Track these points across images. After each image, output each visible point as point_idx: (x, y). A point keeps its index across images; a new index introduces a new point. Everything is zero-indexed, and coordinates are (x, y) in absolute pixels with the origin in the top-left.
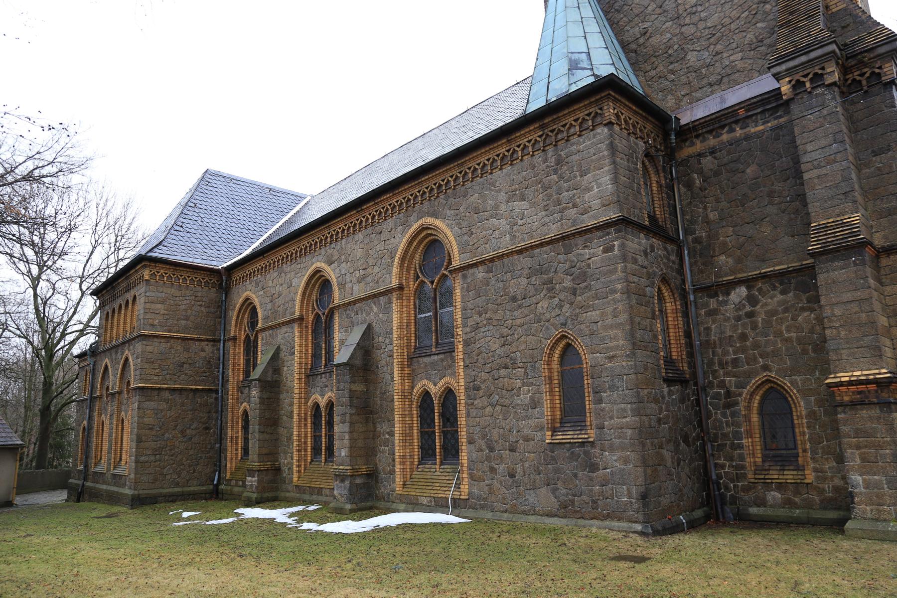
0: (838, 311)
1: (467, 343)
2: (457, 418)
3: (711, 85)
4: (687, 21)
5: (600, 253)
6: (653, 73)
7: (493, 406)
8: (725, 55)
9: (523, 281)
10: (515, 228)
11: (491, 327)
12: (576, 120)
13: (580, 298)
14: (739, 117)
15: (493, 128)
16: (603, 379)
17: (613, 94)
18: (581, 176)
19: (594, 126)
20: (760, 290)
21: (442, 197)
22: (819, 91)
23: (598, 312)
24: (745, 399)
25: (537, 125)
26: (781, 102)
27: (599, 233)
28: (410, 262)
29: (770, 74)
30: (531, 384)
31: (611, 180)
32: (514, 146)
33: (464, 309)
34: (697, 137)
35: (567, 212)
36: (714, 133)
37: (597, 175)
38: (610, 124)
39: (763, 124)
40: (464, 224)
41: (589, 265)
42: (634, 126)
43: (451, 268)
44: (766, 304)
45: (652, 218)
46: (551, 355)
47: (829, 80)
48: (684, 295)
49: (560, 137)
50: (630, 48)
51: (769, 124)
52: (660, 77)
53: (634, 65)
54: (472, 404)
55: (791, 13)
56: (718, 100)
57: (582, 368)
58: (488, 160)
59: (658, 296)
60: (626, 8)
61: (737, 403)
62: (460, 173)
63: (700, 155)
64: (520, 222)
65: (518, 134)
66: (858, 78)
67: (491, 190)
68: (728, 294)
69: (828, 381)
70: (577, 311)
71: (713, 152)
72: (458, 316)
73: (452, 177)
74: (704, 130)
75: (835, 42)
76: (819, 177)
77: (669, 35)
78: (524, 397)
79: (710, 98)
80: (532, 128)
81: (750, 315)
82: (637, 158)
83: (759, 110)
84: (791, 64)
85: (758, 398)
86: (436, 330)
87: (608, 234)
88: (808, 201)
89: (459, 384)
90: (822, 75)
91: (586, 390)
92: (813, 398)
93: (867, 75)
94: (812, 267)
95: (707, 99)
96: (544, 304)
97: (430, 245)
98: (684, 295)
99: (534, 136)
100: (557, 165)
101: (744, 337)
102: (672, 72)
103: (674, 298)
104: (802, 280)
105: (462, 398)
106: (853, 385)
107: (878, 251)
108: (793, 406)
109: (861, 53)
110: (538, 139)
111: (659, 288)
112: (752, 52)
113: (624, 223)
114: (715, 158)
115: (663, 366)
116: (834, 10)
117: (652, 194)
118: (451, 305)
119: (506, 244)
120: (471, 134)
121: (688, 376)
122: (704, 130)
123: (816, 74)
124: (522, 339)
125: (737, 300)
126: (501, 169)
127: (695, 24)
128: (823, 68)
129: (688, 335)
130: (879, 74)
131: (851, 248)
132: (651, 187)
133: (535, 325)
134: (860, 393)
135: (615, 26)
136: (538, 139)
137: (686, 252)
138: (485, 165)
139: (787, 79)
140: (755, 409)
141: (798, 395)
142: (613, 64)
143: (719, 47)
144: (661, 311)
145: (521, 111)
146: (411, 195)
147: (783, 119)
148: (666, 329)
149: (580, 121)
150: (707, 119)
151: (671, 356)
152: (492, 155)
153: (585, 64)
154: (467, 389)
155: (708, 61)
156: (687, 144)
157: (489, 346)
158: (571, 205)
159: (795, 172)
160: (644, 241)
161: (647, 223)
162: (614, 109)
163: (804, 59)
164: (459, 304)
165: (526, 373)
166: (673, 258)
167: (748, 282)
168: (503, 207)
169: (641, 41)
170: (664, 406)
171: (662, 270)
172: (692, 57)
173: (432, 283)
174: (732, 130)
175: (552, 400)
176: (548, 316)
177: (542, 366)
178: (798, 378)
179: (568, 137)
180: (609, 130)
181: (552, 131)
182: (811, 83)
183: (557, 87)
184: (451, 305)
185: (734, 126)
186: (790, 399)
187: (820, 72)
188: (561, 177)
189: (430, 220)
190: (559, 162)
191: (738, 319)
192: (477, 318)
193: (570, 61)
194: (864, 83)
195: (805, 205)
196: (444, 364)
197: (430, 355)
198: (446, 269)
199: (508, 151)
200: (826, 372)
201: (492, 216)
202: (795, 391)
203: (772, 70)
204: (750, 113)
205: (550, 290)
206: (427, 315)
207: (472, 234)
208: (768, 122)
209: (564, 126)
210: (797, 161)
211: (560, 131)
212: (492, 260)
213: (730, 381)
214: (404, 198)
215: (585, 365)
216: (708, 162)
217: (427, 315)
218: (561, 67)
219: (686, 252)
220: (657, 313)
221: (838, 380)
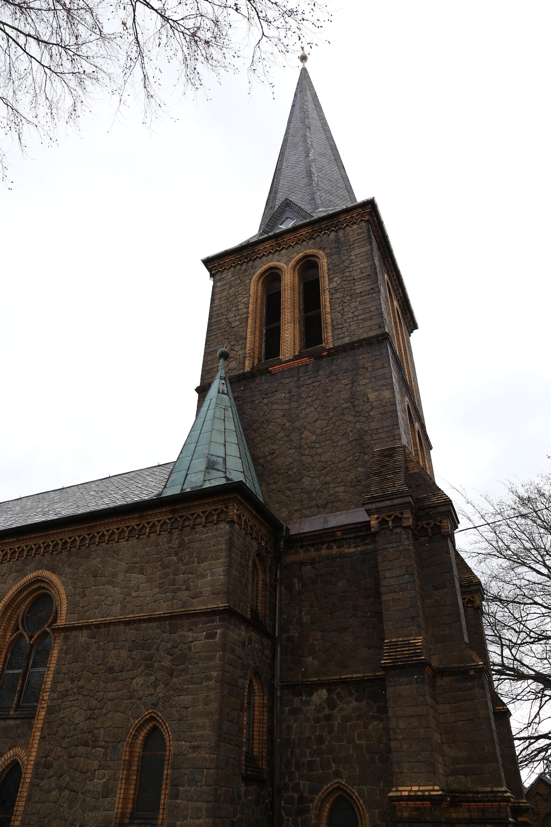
0: (402, 724)
1: (50, 711)
2: (15, 801)
3: (318, 507)
4: (307, 452)
5: (203, 638)
6: (274, 486)
7: (61, 789)
8: (332, 486)
9: (124, 653)
10: (128, 599)
11: (81, 697)
12: (204, 512)
13: (176, 680)
14: (336, 538)
15: (129, 500)
16: (184, 771)
17: (239, 497)
18: (199, 563)
19: (218, 521)
20: (338, 694)
21: (65, 553)
22: (398, 530)
23: (190, 697)
24: (317, 805)
25: (169, 509)
26: (370, 532)
27: (204, 619)
28: (14, 611)
29: (363, 509)
30: (108, 767)
31: (224, 571)
32: (144, 522)
33: (57, 672)
34: (302, 547)
35: (179, 593)
36: (315, 547)
37: (211, 570)
38: (232, 522)
39: (355, 547)
40: (80, 584)
41: (190, 649)
42: (251, 528)
43: (55, 626)
44: (342, 709)
45: (254, 612)
46: (135, 737)
47: (406, 523)
48: (272, 690)
49: (187, 523)
50: (258, 460)
51: (359, 549)
52: (279, 491)
53: (260, 476)
54: (38, 785)
55: (383, 467)
56: (322, 520)
57: (165, 755)
58: (118, 529)
59: (249, 688)
60: (261, 430)
61: (308, 811)
62: (88, 535)
63: (302, 563)
64: (134, 594)
65: (150, 513)
66: (425, 526)
67: (113, 557)
68: (311, 695)
69: (391, 794)
70: (171, 693)
71: (313, 562)
72: (49, 679)
73: (79, 536)
74: (308, 543)
75: (411, 496)
76: (393, 600)
77: (291, 460)
78: (98, 782)
79: (316, 517)
80: (164, 510)
81: (328, 718)
82: (249, 556)
83: (353, 535)
84: (380, 505)
85: (328, 806)
86: (21, 691)
87: (213, 621)
88: (384, 619)
89: (28, 757)
90: (401, 518)
91: (164, 782)
92: (377, 811)
93: (432, 525)
94: (382, 679)
95: (313, 518)
96: (140, 680)
97: (39, 599)
98: (272, 690)
99: (165, 518)
100: (179, 547)
101: (320, 740)
102: (289, 489)
103: (263, 692)
104: (373, 689)
105: (28, 777)
106: (411, 801)
107: (434, 672)
108: (359, 818)
109: (428, 508)
110: (167, 521)
111: (251, 681)
112: (352, 489)
113: (228, 614)
114: (314, 568)
115: (243, 763)
116: (412, 472)
117: (257, 590)
118: (45, 665)
119: (116, 613)
120: (106, 500)
121: (265, 775)
122: (308, 543)
123: (396, 517)
124: (109, 715)
125: (318, 702)
126: (127, 540)
127: (312, 456)
128: (402, 514)
129: (271, 731)
130: (439, 526)
131: (412, 667)
132: (257, 584)
133: (127, 701)
134: (417, 809)
135: (250, 441)
136: (167, 521)
137: (279, 649)
138: (113, 533)
139: (376, 516)
140: (325, 818)
141: (364, 806)
142: (243, 472)
143: (328, 478)
144: (249, 703)
145: (156, 492)
146: (35, 545)
147: (369, 547)
148: (251, 723)
149: (207, 513)
150: (312, 534)
151: (253, 751)
152: (122, 525)
153: (220, 467)
154: (37, 765)
155: (318, 487)
156: (293, 551)
157: (73, 717)
158: (184, 587)
159: (376, 593)
160: (243, 633)
161: (249, 616)
162: (238, 510)
163: (388, 503)
164: (53, 665)
165: (105, 754)
166: (267, 652)
167: (329, 686)
168: (121, 576)
169: (269, 458)
170: (239, 808)
171: (255, 663)
172: (306, 481)
173: (31, 638)
174: (330, 548)
175: (127, 789)
176: (141, 693)
177: (124, 748)
178: (365, 788)
179: (194, 525)
180: (230, 527)
181: (181, 517)
182: (393, 523)
183: (193, 480)
184: (45, 665)
185: (332, 544)
186: (356, 810)
187: (399, 515)
188: (180, 560)
189: (46, 574)
190: (182, 545)
191: (317, 720)
192: (68, 684)
193: (209, 461)
194: (429, 530)
195: (382, 622)
196: (19, 731)
197: (6, 719)
198: (49, 626)
199: (138, 525)
200: (390, 784)
201: (108, 583)
202: (361, 802)
203: (365, 506)
204: (345, 536)
205: (148, 667)
206: (16, 671)
207: (85, 596)
208: (359, 546)
209: (192, 515)
210: (377, 584)
211: (187, 519)
212: (98, 626)
213: (304, 785)
214: (27, 546)
215: (167, 753)
216: (307, 570)
217: (16, 671)
218: (200, 464)
219: (279, 649)
220: (246, 705)
221: (399, 794)
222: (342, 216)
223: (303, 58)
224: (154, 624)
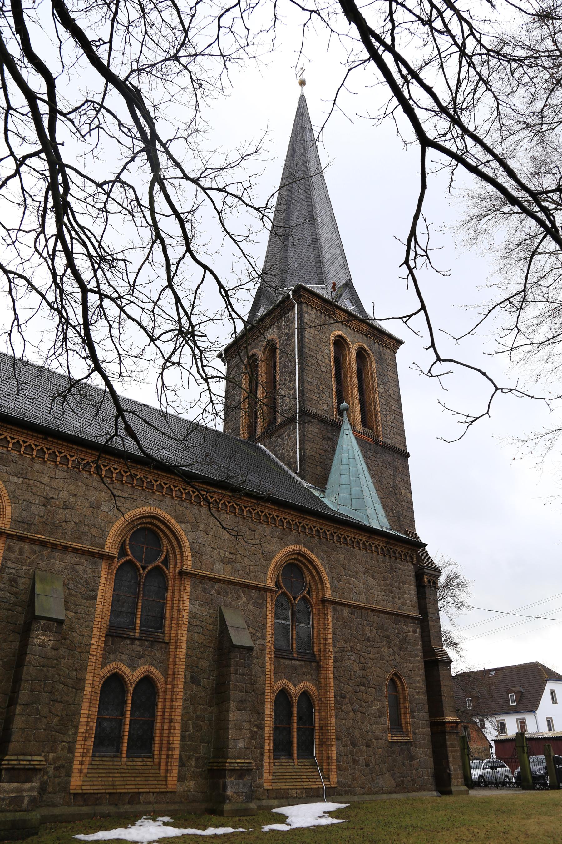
1: (336, 660)
84: (431, 572)
87: (414, 623)
222: (386, 337)
223: (302, 83)
224: (387, 616)
